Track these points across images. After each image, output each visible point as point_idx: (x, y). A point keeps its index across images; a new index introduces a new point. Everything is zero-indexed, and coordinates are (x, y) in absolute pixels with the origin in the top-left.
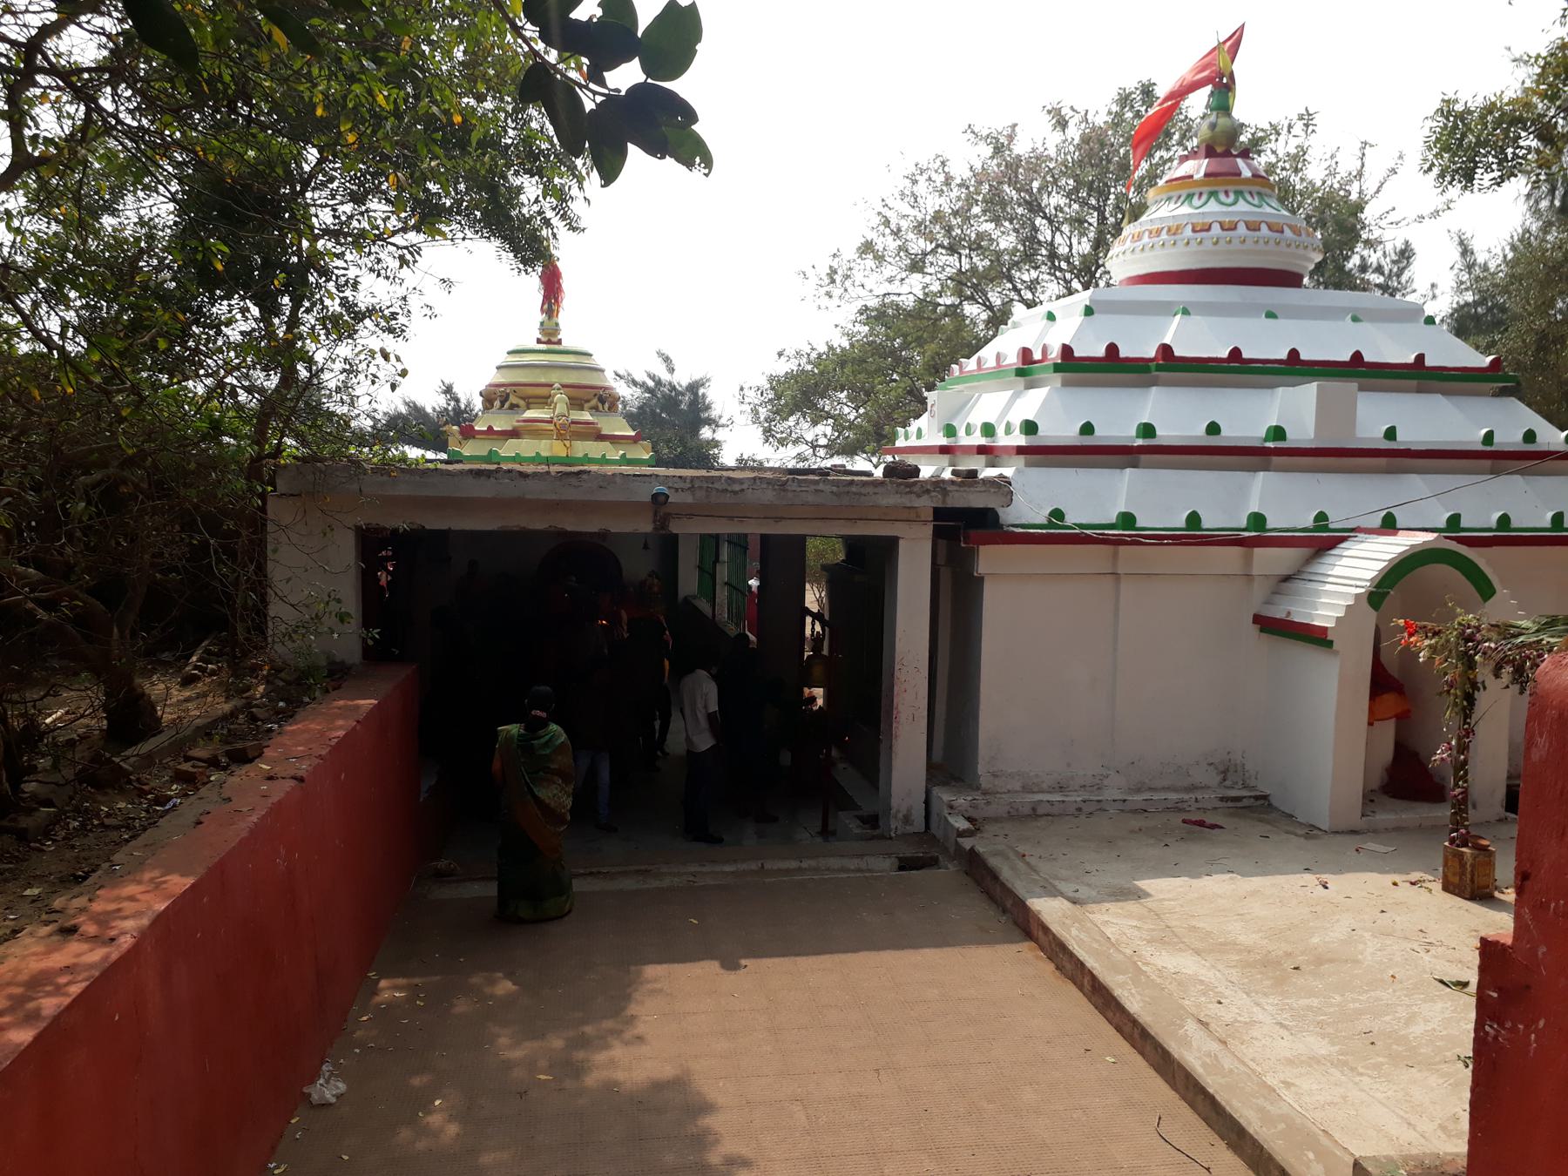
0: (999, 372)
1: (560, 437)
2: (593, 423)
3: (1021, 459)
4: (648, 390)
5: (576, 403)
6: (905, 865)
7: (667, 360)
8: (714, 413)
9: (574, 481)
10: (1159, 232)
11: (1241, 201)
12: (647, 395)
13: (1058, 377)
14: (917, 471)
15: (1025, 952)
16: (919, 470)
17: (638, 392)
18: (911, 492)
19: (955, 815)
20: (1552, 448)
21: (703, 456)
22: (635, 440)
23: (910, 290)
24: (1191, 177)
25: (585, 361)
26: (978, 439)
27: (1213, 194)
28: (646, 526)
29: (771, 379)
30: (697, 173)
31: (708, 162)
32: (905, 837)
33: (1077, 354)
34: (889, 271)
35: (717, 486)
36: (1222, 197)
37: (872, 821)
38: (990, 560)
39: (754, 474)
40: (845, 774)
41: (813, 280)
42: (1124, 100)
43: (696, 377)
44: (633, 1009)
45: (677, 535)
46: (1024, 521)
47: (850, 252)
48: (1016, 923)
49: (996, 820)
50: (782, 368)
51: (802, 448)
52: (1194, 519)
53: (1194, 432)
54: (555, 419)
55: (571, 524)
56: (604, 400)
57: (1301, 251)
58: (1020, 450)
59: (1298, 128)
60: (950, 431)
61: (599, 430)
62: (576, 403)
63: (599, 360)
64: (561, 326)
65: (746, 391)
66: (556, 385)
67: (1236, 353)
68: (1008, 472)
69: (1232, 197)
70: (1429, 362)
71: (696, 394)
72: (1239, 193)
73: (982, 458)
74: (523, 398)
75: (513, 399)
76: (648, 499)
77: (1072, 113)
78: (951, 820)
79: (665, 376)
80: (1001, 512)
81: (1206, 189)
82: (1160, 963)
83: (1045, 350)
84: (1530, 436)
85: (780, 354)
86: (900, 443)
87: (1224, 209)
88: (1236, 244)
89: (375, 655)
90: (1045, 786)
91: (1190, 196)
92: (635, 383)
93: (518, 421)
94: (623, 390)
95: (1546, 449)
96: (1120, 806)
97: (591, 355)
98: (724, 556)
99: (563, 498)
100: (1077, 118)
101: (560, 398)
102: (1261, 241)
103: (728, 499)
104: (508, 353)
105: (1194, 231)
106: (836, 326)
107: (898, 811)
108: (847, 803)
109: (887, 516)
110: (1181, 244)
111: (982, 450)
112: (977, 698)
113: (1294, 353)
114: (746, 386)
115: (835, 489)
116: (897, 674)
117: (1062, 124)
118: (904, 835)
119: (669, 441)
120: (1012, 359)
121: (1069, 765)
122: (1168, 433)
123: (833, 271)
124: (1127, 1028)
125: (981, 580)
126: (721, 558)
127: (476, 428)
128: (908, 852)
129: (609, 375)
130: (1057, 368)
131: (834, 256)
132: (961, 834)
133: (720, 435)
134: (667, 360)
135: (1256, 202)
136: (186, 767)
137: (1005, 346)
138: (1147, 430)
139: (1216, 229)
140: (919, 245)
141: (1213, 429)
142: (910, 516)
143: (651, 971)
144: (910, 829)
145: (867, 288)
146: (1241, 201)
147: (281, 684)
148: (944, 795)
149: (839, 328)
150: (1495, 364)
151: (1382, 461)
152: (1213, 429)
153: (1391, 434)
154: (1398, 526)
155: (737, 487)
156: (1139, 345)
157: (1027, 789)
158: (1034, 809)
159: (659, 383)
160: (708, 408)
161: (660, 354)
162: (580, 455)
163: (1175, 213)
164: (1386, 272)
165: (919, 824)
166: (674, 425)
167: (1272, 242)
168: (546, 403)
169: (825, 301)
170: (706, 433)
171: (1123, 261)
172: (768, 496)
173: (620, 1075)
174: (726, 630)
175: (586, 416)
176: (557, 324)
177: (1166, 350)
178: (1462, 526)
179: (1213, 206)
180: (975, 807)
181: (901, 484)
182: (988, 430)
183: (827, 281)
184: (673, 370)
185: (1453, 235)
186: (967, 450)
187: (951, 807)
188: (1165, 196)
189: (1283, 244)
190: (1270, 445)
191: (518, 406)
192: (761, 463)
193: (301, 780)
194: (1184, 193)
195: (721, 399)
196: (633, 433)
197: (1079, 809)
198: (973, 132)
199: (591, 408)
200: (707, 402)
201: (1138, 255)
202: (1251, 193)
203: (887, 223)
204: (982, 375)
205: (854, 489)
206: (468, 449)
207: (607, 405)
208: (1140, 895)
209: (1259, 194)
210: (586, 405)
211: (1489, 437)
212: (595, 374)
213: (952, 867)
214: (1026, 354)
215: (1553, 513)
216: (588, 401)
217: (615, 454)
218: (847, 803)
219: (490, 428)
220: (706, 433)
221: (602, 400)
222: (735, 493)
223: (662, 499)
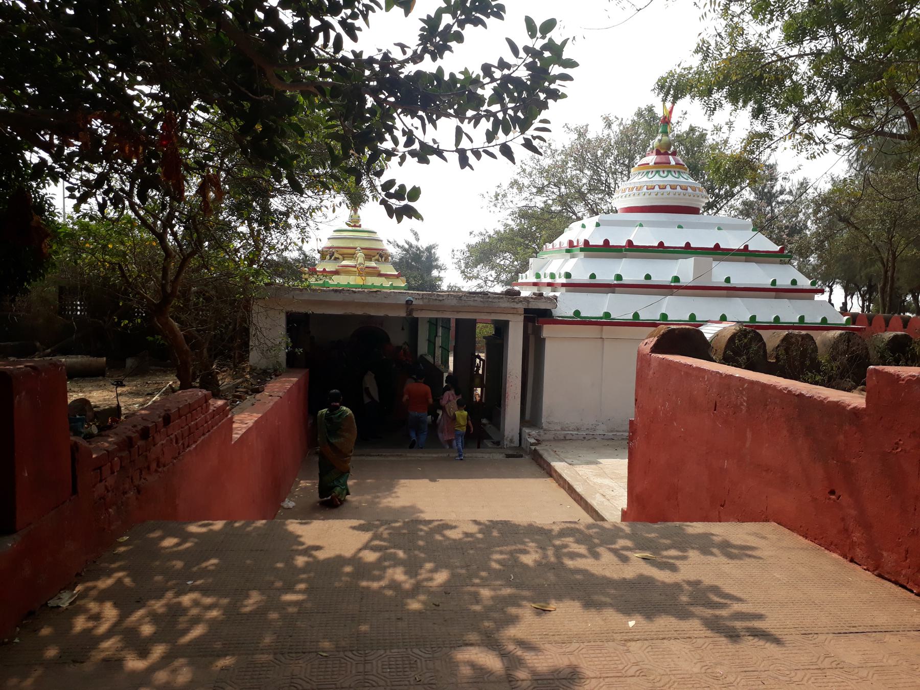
0: (559, 250)
1: (360, 275)
2: (376, 268)
3: (564, 289)
4: (405, 250)
5: (368, 257)
6: (508, 456)
7: (416, 234)
8: (440, 263)
9: (374, 294)
10: (633, 189)
11: (670, 175)
12: (404, 252)
13: (583, 253)
14: (519, 293)
15: (550, 483)
16: (520, 293)
17: (400, 250)
18: (514, 302)
19: (531, 435)
20: (804, 288)
21: (433, 285)
22: (397, 277)
23: (539, 202)
24: (649, 164)
25: (372, 235)
26: (548, 280)
27: (658, 172)
28: (403, 314)
29: (468, 246)
30: (420, 221)
31: (422, 219)
32: (511, 448)
33: (590, 244)
34: (526, 194)
35: (433, 297)
36: (661, 173)
37: (497, 443)
38: (548, 331)
39: (457, 295)
40: (490, 429)
41: (488, 199)
42: (640, 114)
43: (431, 244)
44: (396, 490)
45: (417, 318)
46: (563, 315)
47: (506, 185)
48: (547, 473)
49: (548, 441)
50: (474, 241)
51: (480, 281)
52: (636, 315)
53: (640, 278)
54: (358, 266)
55: (373, 313)
56: (382, 256)
57: (696, 198)
58: (563, 285)
59: (725, 128)
60: (538, 276)
61: (380, 271)
62: (368, 257)
63: (379, 235)
64: (361, 218)
65: (455, 252)
66: (358, 248)
67: (661, 244)
68: (557, 294)
69: (666, 173)
70: (750, 248)
71: (430, 253)
72: (669, 172)
73: (550, 288)
74: (341, 255)
75: (336, 255)
76: (405, 303)
77: (615, 119)
78: (529, 439)
79: (414, 243)
80: (553, 311)
81: (654, 170)
82: (595, 481)
83: (578, 241)
84: (794, 282)
85: (471, 233)
86: (520, 281)
87: (662, 179)
88: (665, 195)
89: (292, 362)
90: (571, 429)
91: (648, 173)
92: (398, 246)
93: (339, 266)
94: (391, 250)
95: (802, 288)
96: (603, 437)
97: (376, 233)
98: (440, 334)
99: (370, 301)
100: (618, 122)
101: (360, 256)
102: (677, 194)
103: (437, 303)
104: (335, 231)
105: (647, 189)
106: (499, 221)
107: (508, 437)
108: (488, 437)
109: (504, 311)
110: (641, 195)
111: (549, 285)
112: (542, 390)
113: (688, 244)
114: (455, 249)
115: (482, 300)
116: (508, 378)
117: (609, 125)
118: (510, 447)
119: (415, 277)
120: (566, 245)
121: (582, 420)
122: (627, 279)
123: (497, 195)
124: (577, 498)
125: (544, 339)
126: (438, 335)
127: (317, 269)
128: (510, 452)
129: (385, 242)
130: (582, 250)
131: (498, 186)
132: (532, 444)
133: (442, 274)
134: (416, 234)
135: (677, 176)
136: (238, 393)
137: (563, 240)
138: (619, 277)
139: (657, 188)
140: (540, 181)
141: (648, 277)
142: (514, 312)
143: (402, 481)
144: (513, 445)
145: (514, 203)
146: (670, 175)
147: (256, 374)
148: (526, 430)
149: (500, 222)
150: (782, 250)
151: (725, 292)
152: (648, 277)
153: (728, 280)
154: (728, 320)
155: (441, 298)
156: (618, 239)
157: (563, 429)
158: (565, 437)
159: (411, 246)
160: (436, 260)
161: (412, 231)
162: (370, 284)
163: (640, 180)
164: (794, 194)
165: (516, 443)
166: (418, 269)
167: (682, 194)
168: (353, 257)
169: (493, 208)
170: (435, 273)
171: (619, 201)
172: (454, 302)
173: (391, 505)
174: (440, 368)
175: (373, 264)
176: (359, 217)
177: (630, 243)
178: (757, 320)
179: (657, 178)
180: (539, 435)
181: (509, 298)
182: (552, 276)
183: (494, 199)
184: (419, 239)
185: (828, 175)
186: (543, 284)
187: (529, 435)
188: (637, 172)
189: (687, 195)
190: (673, 284)
191: (338, 258)
192: (459, 289)
193: (281, 397)
194: (645, 171)
195: (443, 256)
196: (396, 273)
197: (584, 438)
198: (567, 127)
199: (376, 260)
200: (436, 257)
201: (624, 198)
202: (675, 172)
203: (524, 171)
204: (554, 251)
205: (490, 300)
206: (312, 280)
207: (383, 259)
208: (597, 463)
209: (679, 172)
210: (373, 258)
211: (774, 282)
212: (378, 242)
213: (527, 457)
214: (571, 242)
215: (799, 316)
216: (374, 256)
217: (387, 283)
218: (488, 437)
219: (324, 269)
220: (435, 273)
221: (381, 256)
222: (440, 300)
223: (410, 302)
